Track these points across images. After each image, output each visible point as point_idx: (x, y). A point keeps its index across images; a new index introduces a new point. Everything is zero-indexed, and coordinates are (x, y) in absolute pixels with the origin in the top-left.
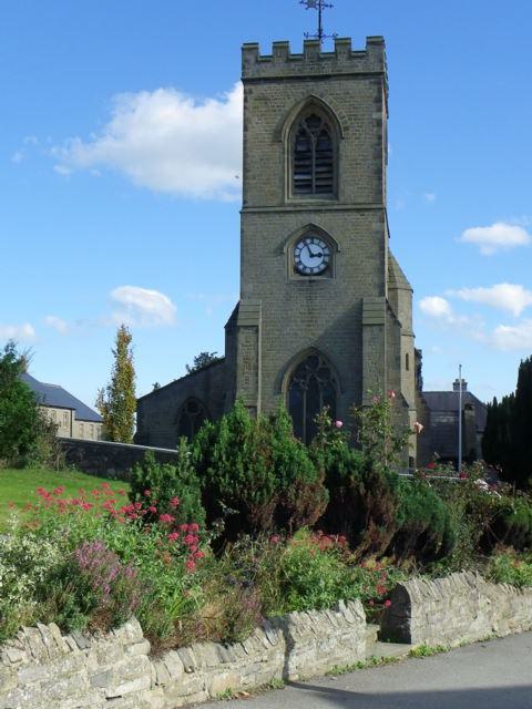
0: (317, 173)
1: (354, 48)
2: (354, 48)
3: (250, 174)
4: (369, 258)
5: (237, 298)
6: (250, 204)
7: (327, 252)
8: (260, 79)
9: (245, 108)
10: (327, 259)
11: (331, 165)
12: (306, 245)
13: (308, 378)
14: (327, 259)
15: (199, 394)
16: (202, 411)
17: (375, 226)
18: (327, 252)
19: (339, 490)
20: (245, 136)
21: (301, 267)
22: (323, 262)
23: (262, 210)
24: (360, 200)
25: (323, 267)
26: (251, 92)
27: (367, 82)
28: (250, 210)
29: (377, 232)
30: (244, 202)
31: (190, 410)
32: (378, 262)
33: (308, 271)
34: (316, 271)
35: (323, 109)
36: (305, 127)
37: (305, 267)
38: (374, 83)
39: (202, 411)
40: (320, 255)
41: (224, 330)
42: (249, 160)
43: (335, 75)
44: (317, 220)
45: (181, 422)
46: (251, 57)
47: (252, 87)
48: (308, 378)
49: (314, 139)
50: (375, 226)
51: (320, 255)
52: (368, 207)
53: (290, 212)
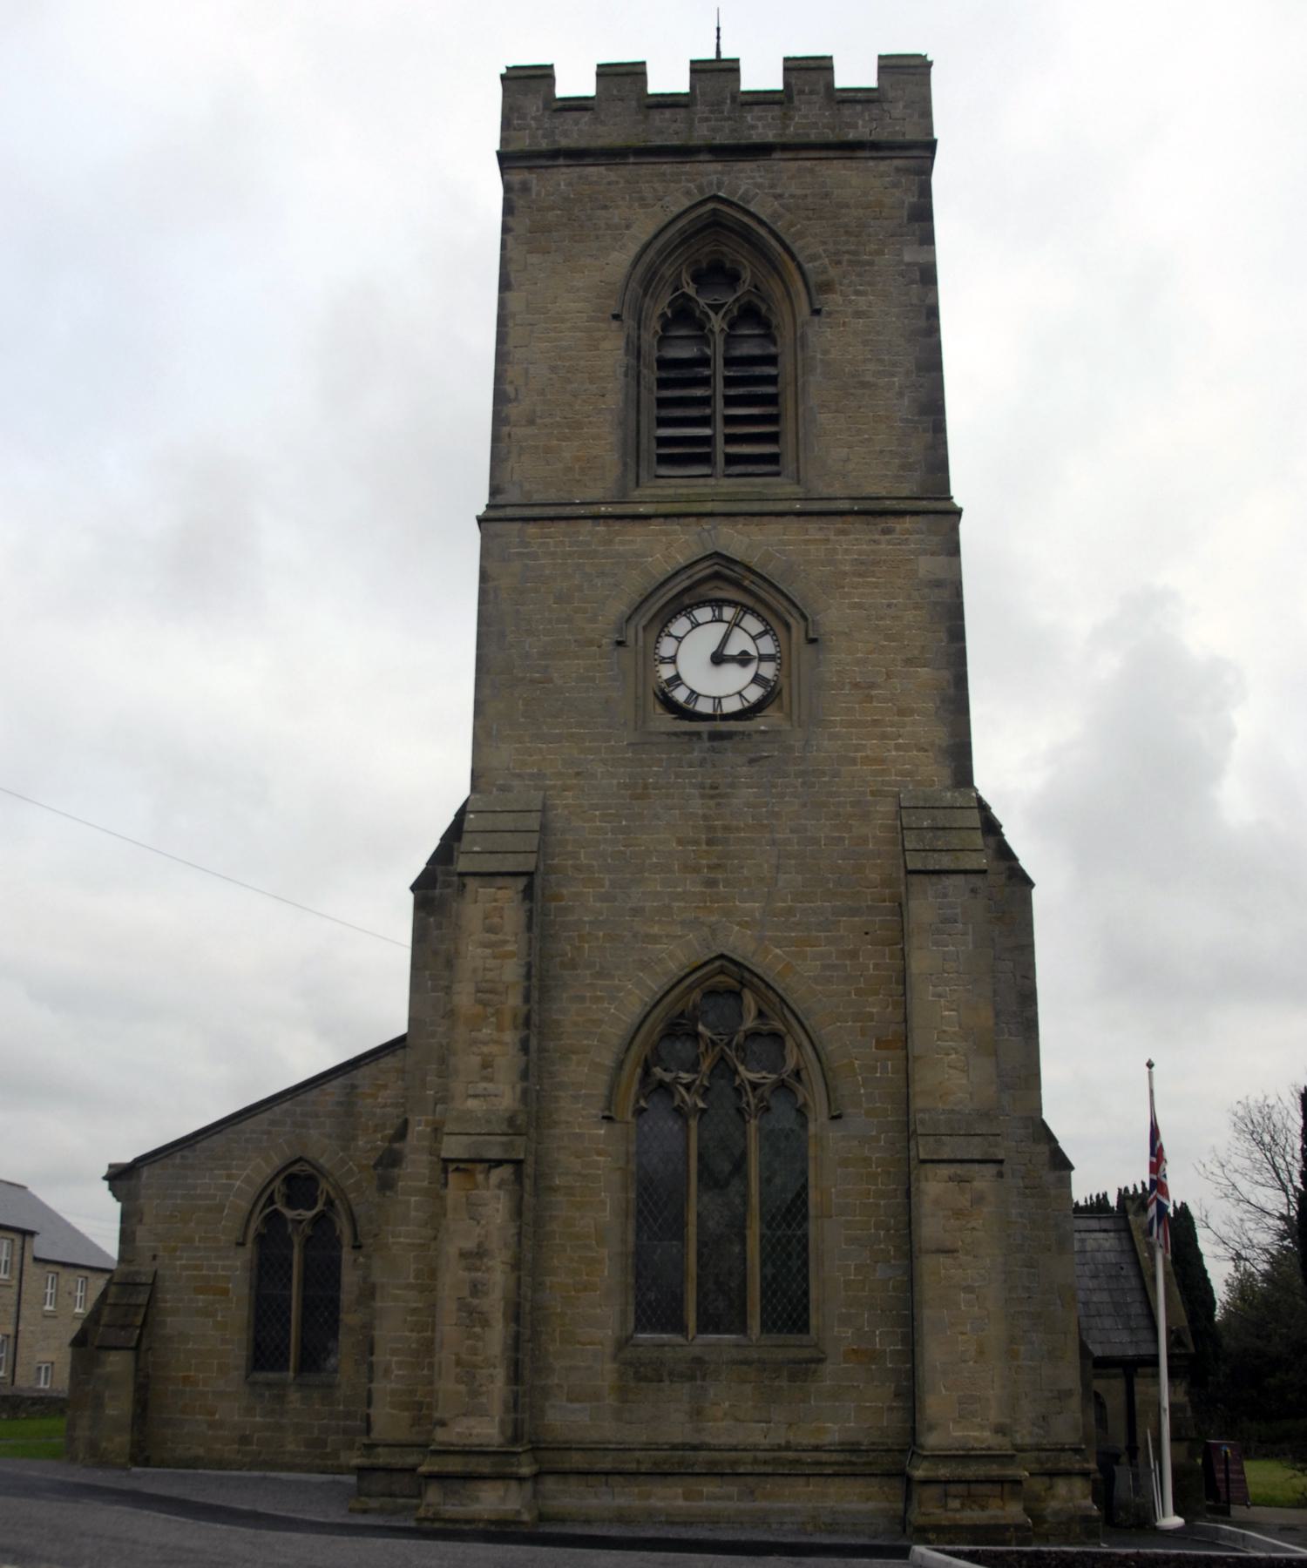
0: (730, 420)
1: (841, 81)
2: (841, 81)
3: (512, 410)
4: (909, 662)
5: (460, 790)
6: (513, 495)
7: (767, 645)
8: (555, 154)
9: (506, 229)
10: (768, 670)
11: (772, 400)
12: (762, 658)
13: (705, 1066)
14: (768, 670)
15: (321, 1147)
16: (330, 1203)
17: (927, 566)
18: (767, 645)
19: (651, 783)
20: (502, 304)
21: (680, 695)
22: (757, 679)
23: (551, 512)
24: (871, 490)
25: (754, 694)
26: (525, 188)
27: (883, 166)
28: (509, 512)
29: (938, 584)
30: (494, 491)
31: (291, 1202)
32: (946, 674)
33: (704, 707)
34: (732, 705)
35: (746, 235)
36: (690, 290)
37: (694, 695)
38: (907, 171)
39: (330, 1203)
40: (743, 659)
41: (409, 898)
42: (512, 372)
43: (785, 147)
44: (736, 540)
45: (261, 1239)
46: (533, 106)
47: (532, 178)
48: (705, 1066)
49: (717, 323)
50: (927, 566)
51: (743, 659)
52: (903, 505)
53: (711, 515)
